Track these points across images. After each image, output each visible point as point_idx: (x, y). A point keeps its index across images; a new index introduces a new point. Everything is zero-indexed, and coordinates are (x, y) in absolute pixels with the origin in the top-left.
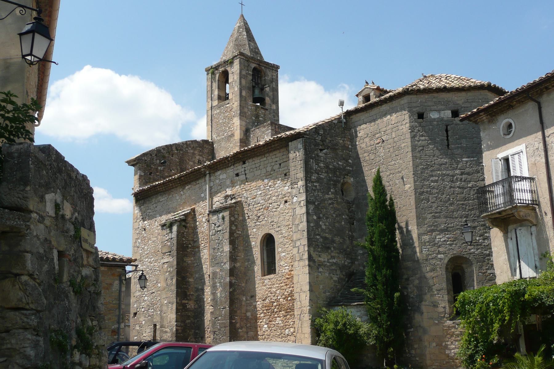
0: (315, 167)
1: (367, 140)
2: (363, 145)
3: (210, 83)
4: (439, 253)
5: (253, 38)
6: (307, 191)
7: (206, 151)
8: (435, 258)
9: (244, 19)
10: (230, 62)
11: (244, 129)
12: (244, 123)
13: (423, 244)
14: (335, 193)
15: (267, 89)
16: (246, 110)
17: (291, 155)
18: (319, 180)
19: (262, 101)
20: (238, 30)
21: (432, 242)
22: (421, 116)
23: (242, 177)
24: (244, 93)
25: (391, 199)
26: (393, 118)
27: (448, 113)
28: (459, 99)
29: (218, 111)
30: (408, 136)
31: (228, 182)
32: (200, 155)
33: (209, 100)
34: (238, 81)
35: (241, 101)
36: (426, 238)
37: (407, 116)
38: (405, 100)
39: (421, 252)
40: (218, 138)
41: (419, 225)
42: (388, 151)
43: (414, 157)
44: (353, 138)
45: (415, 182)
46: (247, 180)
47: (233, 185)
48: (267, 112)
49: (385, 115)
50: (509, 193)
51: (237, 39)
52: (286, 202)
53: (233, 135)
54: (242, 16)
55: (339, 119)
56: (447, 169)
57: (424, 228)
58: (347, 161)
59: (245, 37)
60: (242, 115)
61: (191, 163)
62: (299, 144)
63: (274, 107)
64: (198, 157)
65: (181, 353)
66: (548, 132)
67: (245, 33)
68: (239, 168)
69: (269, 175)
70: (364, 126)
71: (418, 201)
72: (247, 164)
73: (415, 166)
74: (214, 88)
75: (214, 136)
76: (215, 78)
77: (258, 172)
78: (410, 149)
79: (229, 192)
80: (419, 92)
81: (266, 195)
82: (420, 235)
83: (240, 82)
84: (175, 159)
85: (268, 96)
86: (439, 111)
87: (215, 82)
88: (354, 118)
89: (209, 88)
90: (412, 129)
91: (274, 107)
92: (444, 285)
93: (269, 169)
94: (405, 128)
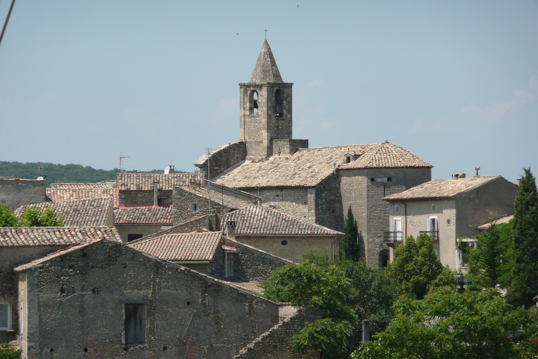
0: (320, 202)
1: (347, 186)
2: (345, 188)
3: (242, 96)
4: (376, 247)
5: (275, 64)
6: (316, 215)
7: (241, 149)
8: (375, 250)
9: (268, 45)
10: (261, 87)
11: (270, 138)
12: (270, 134)
13: (369, 243)
14: (330, 214)
15: (284, 102)
16: (271, 124)
17: (309, 195)
18: (322, 208)
19: (281, 115)
20: (264, 56)
21: (374, 242)
22: (372, 180)
23: (280, 198)
24: (270, 113)
25: (356, 222)
26: (359, 178)
27: (386, 179)
28: (392, 173)
29: (249, 120)
30: (366, 190)
31: (272, 198)
32: (238, 154)
33: (242, 109)
34: (266, 104)
35: (268, 118)
36: (371, 240)
37: (366, 180)
38: (365, 171)
39: (368, 246)
40: (249, 140)
41: (368, 234)
42: (355, 195)
43: (368, 201)
44: (339, 182)
45: (367, 213)
46: (283, 200)
47: (275, 200)
48: (284, 121)
49: (356, 176)
50: (395, 237)
51: (263, 65)
52: (305, 217)
53: (261, 142)
54: (266, 41)
55: (333, 174)
56: (382, 207)
57: (371, 235)
58: (336, 195)
59: (269, 63)
60: (269, 129)
61: (233, 160)
62: (313, 191)
63: (289, 116)
64: (236, 155)
65: (56, 257)
66: (407, 217)
67: (269, 59)
68: (279, 192)
69: (297, 201)
70: (345, 178)
71: (368, 222)
72: (283, 192)
73: (368, 205)
74: (246, 100)
75: (247, 137)
76: (247, 93)
77: (290, 198)
78: (366, 196)
79: (272, 204)
80: (369, 168)
81: (294, 211)
82: (368, 239)
83: (268, 112)
84: (224, 159)
85: (285, 109)
86: (381, 178)
87: (247, 96)
88: (341, 172)
89: (242, 100)
90: (368, 186)
91: (289, 116)
92: (378, 262)
93: (296, 197)
94: (365, 185)
